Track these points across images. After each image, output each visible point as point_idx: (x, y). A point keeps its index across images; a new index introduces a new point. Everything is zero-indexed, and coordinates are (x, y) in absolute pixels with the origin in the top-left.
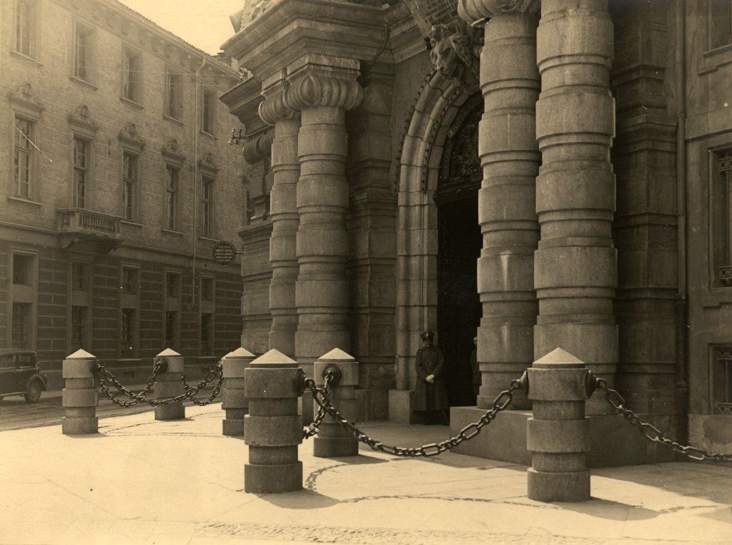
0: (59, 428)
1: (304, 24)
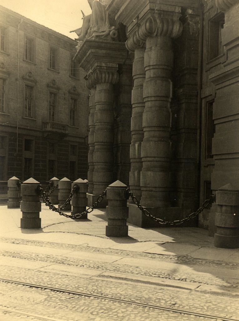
0: (7, 206)
1: (93, 50)
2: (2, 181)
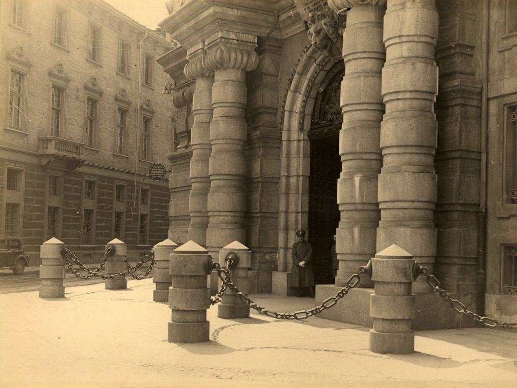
0: (37, 293)
1: (218, 9)
2: (87, 246)
